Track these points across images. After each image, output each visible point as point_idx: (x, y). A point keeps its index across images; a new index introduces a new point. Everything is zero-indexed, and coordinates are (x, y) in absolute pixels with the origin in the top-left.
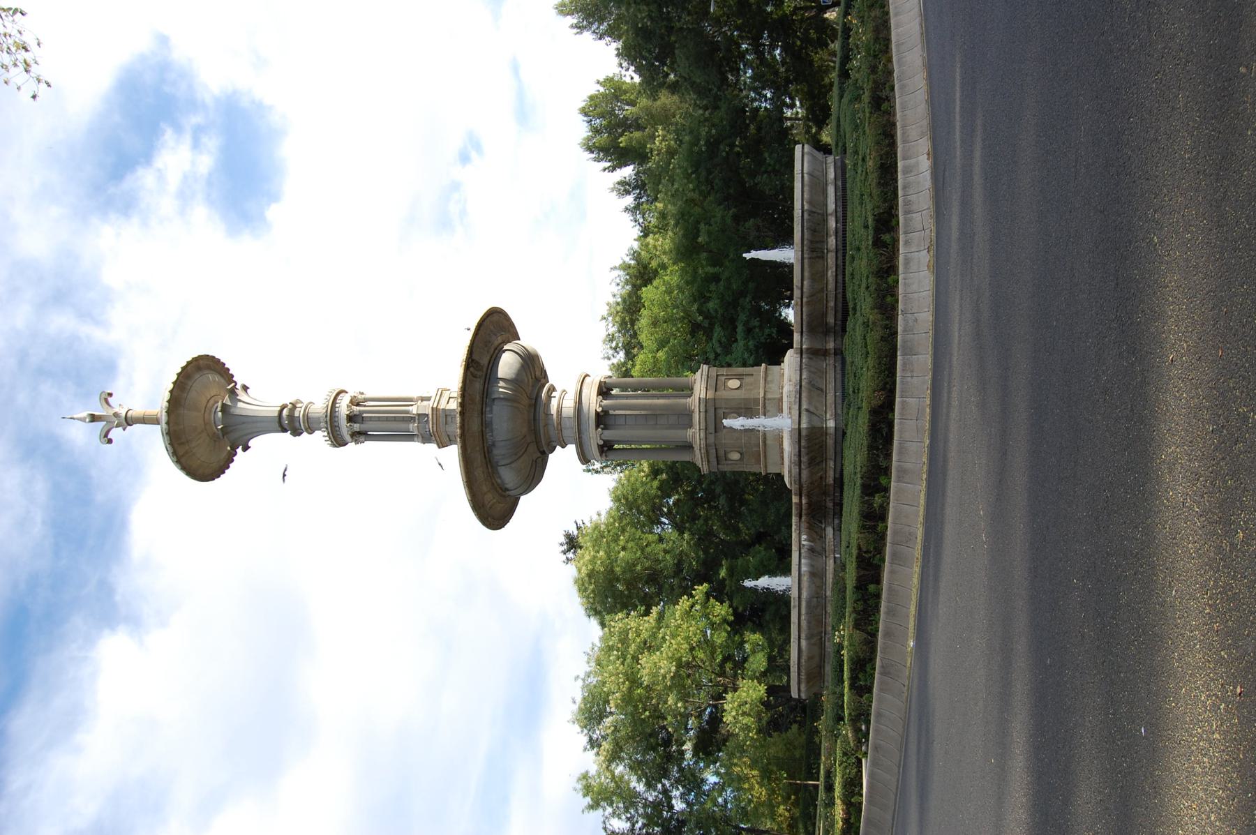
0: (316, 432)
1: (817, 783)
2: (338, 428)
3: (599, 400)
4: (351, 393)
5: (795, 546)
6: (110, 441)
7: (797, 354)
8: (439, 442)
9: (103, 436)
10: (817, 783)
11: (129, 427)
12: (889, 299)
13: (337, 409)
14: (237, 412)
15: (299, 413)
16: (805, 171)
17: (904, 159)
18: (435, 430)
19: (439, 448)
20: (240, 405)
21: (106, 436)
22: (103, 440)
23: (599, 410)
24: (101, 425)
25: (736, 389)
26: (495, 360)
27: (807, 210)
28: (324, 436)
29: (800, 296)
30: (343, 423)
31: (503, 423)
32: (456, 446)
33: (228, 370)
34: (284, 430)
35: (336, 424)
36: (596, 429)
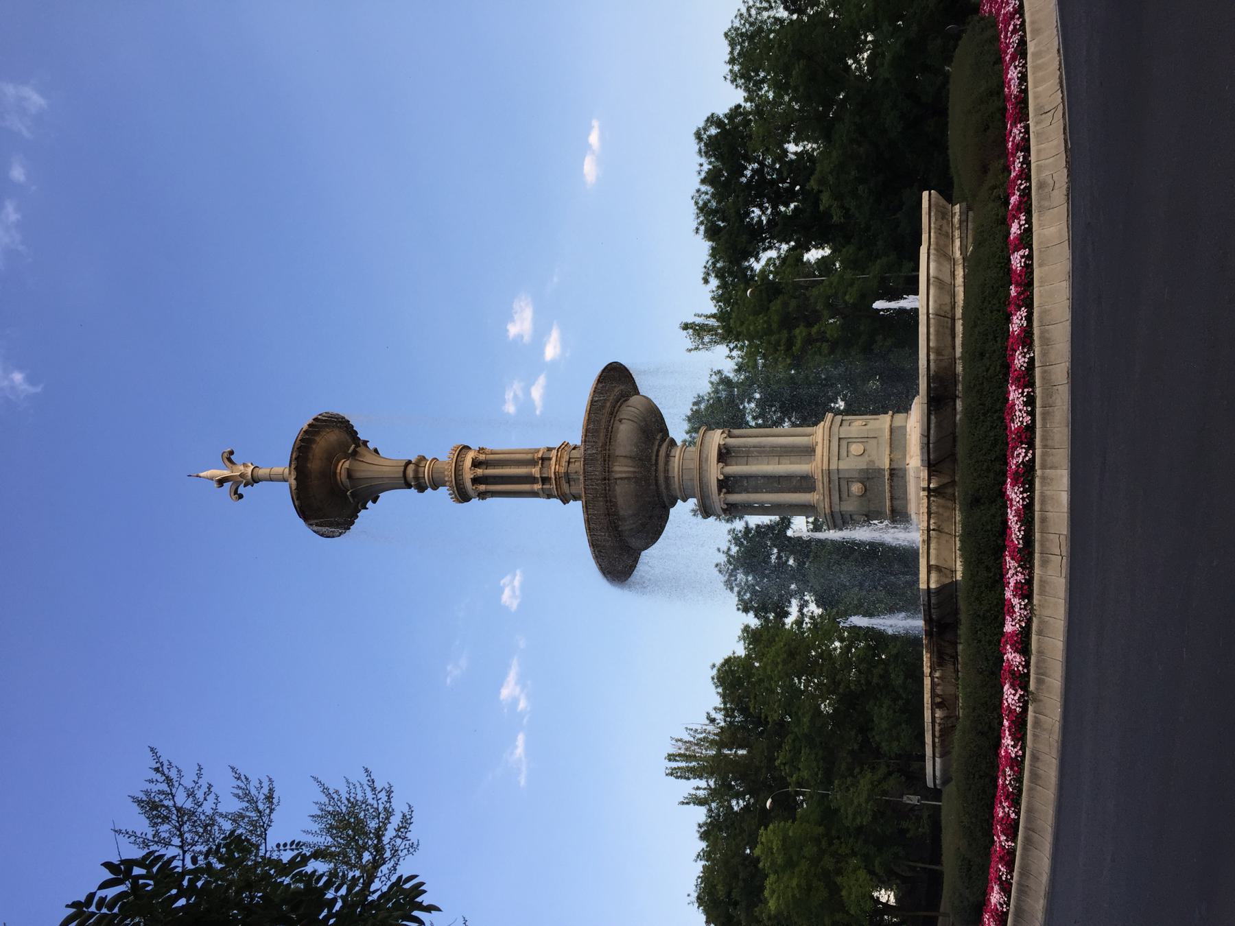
0: (440, 488)
1: (940, 804)
2: (464, 490)
3: (719, 468)
4: (475, 446)
5: (923, 557)
6: (241, 496)
7: (923, 466)
8: (564, 499)
9: (232, 494)
10: (940, 804)
11: (255, 484)
12: (1027, 679)
13: (461, 482)
14: (362, 475)
15: (426, 471)
16: (931, 311)
17: (1040, 265)
18: (560, 493)
19: (565, 504)
20: (363, 466)
21: (236, 493)
22: (234, 497)
23: (721, 477)
24: (227, 485)
25: (859, 455)
26: (619, 407)
27: (933, 348)
28: (452, 498)
29: (932, 756)
30: (468, 484)
31: (623, 494)
32: (581, 502)
33: (353, 426)
34: (409, 486)
35: (460, 473)
36: (719, 494)
